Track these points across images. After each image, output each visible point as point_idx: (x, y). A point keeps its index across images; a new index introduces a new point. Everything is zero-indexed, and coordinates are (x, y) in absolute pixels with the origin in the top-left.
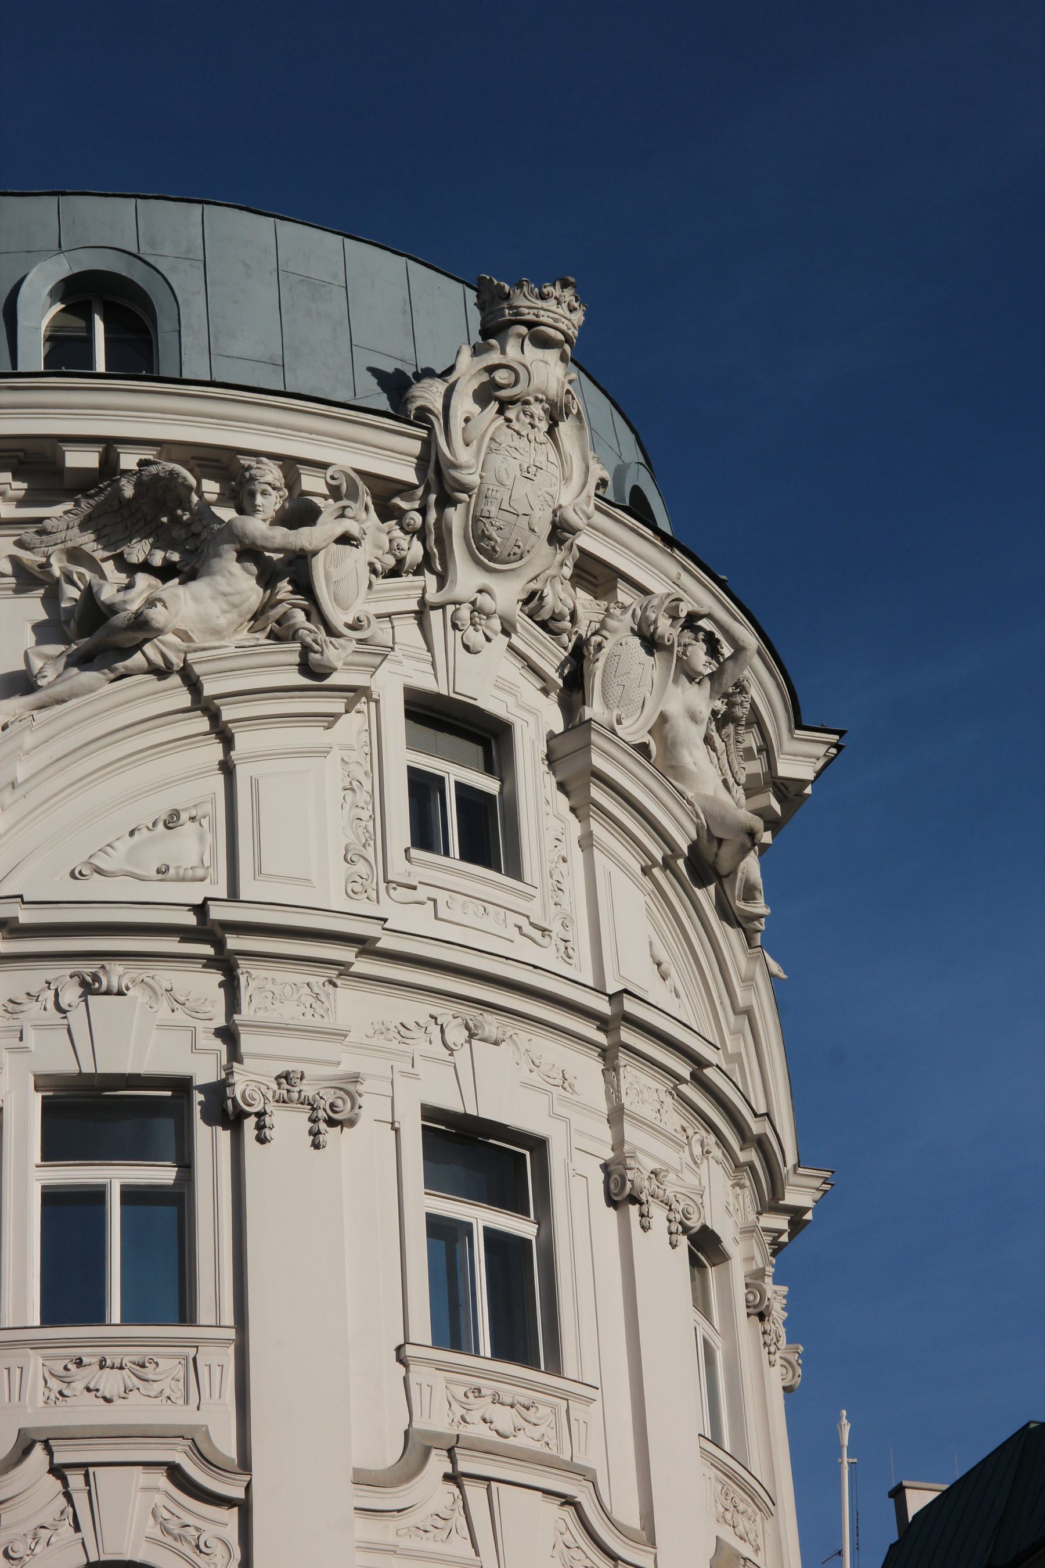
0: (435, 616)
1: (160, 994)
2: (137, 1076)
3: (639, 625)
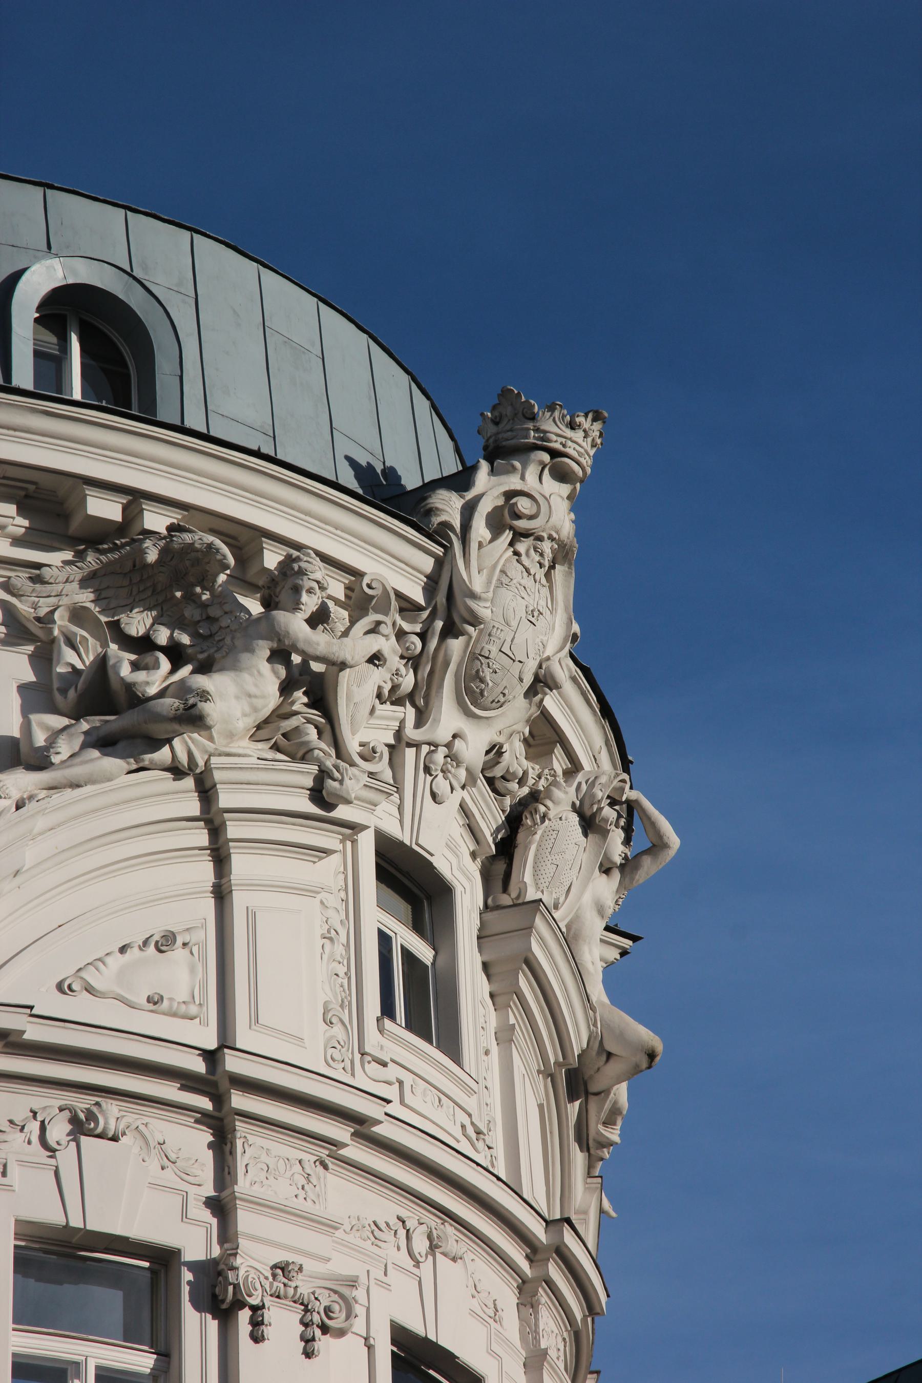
0: (410, 753)
1: (152, 1147)
2: (124, 1240)
3: (581, 802)
